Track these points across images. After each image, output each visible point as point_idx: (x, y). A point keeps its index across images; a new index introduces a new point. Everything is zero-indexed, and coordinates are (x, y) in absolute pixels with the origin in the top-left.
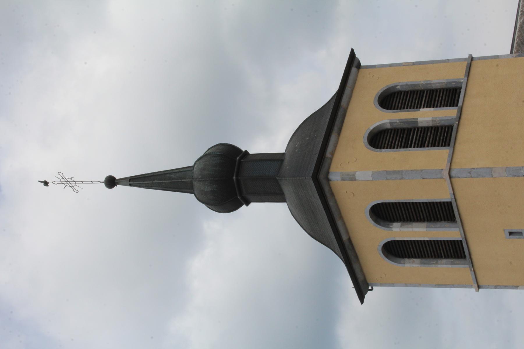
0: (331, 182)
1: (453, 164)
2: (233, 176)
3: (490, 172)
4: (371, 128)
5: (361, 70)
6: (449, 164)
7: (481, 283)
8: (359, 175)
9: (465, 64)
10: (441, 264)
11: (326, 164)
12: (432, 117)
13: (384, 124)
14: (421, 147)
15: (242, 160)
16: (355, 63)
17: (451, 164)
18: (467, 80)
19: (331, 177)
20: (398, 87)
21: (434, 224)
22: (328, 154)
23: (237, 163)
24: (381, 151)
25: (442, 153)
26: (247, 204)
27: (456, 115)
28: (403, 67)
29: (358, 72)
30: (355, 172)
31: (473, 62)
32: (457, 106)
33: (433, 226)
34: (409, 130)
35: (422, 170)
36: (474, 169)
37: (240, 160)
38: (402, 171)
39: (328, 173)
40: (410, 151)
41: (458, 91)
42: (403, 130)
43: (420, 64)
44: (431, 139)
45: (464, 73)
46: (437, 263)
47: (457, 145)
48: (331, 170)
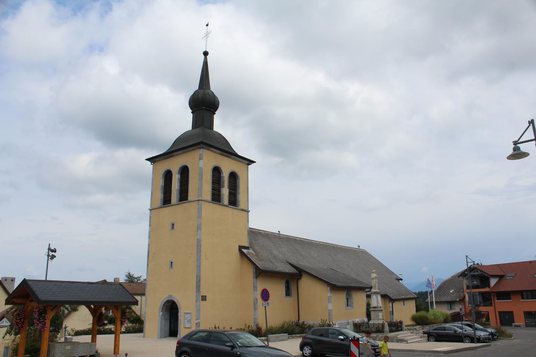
0: (199, 149)
3: (200, 217)
7: (152, 211)
8: (201, 161)
9: (246, 209)
11: (207, 147)
19: (202, 149)
22: (211, 149)
29: (246, 164)
30: (203, 160)
32: (229, 205)
34: (220, 184)
37: (211, 110)
38: (202, 180)
39: (203, 148)
41: (235, 206)
42: (220, 181)
44: (215, 193)
47: (212, 204)
48: (204, 150)
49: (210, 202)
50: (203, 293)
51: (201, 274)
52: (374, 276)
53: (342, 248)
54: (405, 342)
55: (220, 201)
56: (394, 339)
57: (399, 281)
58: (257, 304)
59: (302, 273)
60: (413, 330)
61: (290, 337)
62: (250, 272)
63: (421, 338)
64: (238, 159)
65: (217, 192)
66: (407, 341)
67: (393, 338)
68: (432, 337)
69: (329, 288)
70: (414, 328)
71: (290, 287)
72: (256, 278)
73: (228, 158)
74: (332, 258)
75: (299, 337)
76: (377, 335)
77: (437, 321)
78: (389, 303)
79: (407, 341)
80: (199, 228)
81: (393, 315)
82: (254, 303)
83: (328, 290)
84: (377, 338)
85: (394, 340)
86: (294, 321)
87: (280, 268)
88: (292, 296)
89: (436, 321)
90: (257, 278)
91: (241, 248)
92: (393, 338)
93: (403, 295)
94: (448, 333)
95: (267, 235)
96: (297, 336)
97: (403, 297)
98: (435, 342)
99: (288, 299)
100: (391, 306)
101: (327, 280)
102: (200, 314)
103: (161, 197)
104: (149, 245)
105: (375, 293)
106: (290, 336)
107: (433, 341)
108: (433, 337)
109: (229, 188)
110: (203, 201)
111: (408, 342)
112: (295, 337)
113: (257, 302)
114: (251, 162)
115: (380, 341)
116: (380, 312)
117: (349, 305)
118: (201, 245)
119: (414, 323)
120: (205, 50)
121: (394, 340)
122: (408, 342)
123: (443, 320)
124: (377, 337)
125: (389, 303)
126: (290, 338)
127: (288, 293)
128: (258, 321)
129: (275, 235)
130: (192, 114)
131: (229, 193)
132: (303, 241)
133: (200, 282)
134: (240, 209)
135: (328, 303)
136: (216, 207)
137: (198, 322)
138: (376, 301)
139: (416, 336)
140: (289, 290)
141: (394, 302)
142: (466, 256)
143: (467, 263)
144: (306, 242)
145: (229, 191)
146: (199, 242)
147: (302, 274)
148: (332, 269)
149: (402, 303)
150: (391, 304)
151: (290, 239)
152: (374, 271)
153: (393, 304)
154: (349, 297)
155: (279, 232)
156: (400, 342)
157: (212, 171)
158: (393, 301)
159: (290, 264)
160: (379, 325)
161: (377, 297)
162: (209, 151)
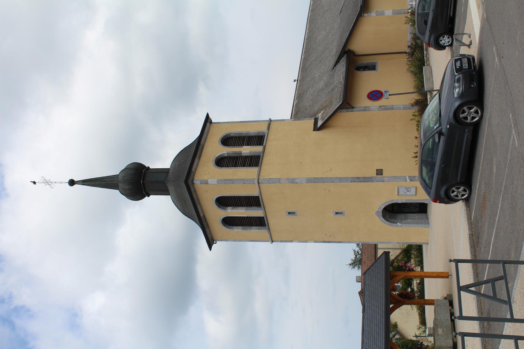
1: (260, 176)
2: (141, 181)
3: (279, 181)
4: (217, 156)
7: (273, 240)
8: (210, 181)
11: (192, 175)
16: (209, 121)
17: (259, 176)
18: (268, 132)
19: (195, 182)
20: (232, 134)
22: (193, 170)
27: (262, 150)
29: (210, 125)
30: (208, 180)
32: (263, 145)
34: (237, 157)
36: (271, 179)
38: (233, 179)
39: (193, 180)
41: (263, 137)
42: (234, 157)
44: (249, 162)
49: (260, 169)
50: (374, 174)
55: (258, 156)
58: (385, 106)
61: (427, 63)
62: (345, 116)
65: (247, 160)
69: (365, 15)
72: (353, 108)
74: (326, 12)
75: (427, 52)
80: (292, 181)
83: (368, 16)
86: (407, 59)
91: (316, 128)
96: (426, 54)
99: (379, 67)
101: (355, 17)
110: (260, 178)
112: (427, 57)
113: (384, 106)
120: (68, 183)
126: (429, 63)
127: (372, 67)
131: (248, 146)
133: (359, 177)
134: (268, 131)
135: (384, 15)
136: (266, 160)
137: (409, 179)
144: (306, 46)
146: (310, 181)
147: (348, 50)
151: (303, 67)
155: (295, 81)
159: (335, 66)
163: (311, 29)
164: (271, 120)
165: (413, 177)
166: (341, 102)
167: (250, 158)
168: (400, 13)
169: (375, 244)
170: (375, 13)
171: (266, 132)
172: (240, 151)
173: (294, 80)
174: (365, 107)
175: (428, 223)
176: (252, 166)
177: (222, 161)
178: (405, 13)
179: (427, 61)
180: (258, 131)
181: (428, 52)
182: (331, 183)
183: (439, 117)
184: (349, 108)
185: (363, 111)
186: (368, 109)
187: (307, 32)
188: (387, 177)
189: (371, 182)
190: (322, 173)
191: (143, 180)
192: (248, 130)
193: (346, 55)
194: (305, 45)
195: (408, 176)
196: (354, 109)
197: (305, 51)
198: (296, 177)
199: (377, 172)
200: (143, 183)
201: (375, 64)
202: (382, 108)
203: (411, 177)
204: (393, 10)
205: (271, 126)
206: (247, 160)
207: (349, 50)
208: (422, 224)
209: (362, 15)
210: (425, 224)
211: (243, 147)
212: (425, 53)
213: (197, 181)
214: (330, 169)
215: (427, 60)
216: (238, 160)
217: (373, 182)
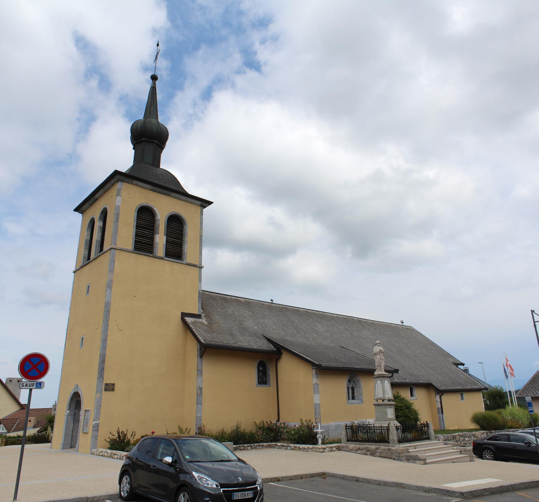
0: (117, 183)
1: (119, 251)
2: (144, 138)
3: (112, 271)
4: (154, 209)
5: (199, 208)
6: (120, 249)
7: (76, 273)
8: (119, 198)
9: (198, 264)
10: (85, 251)
11: (128, 180)
12: (158, 243)
13: (157, 216)
14: (136, 234)
15: (155, 144)
16: (204, 204)
17: (120, 250)
18: (184, 264)
19: (120, 183)
20: (185, 226)
21: (99, 244)
22: (135, 182)
23: (154, 141)
24: (135, 212)
25: (130, 244)
26: (134, 149)
27: (158, 255)
28: (199, 230)
29: (199, 205)
30: (121, 196)
31: (198, 268)
32: (165, 257)
33: (97, 244)
34: (153, 230)
35: (117, 233)
36: (114, 262)
37: (155, 142)
38: (118, 222)
39: (122, 181)
40: (134, 228)
41: (179, 259)
42: (153, 227)
43: (200, 239)
44: (144, 241)
45: (190, 263)
46: (85, 248)
47: (135, 254)
48: (124, 183)
49: (131, 252)
50: (108, 380)
51: (107, 352)
52: (378, 350)
53: (374, 323)
54: (420, 462)
55: (152, 252)
56: (401, 455)
57: (457, 367)
58: (202, 395)
59: (282, 351)
60: (471, 437)
61: (248, 446)
62: (193, 349)
63: (461, 454)
64: (193, 201)
65: (148, 240)
66: (425, 460)
67: (400, 453)
68: (487, 452)
69: (314, 370)
70: (473, 435)
71: (267, 371)
72: (201, 357)
73: (180, 201)
74: (351, 334)
75: (266, 447)
76: (377, 447)
77: (517, 424)
78: (436, 395)
79: (425, 460)
80: (109, 286)
81: (442, 413)
82: (197, 393)
83: (313, 374)
84: (377, 453)
85: (402, 457)
86: (267, 422)
87: (243, 343)
88: (270, 384)
89: (515, 424)
90: (203, 358)
91: (184, 315)
92: (400, 453)
93: (460, 384)
94: (515, 446)
95: (226, 299)
96: (263, 446)
97: (460, 387)
98: (493, 460)
99: (263, 388)
100: (439, 400)
101: (312, 359)
102: (100, 412)
103: (84, 254)
104: (69, 318)
105: (379, 377)
106: (249, 445)
107: (491, 459)
108: (490, 452)
109: (167, 235)
110: (117, 251)
111: (427, 461)
112: (258, 447)
113: (202, 393)
114: (206, 203)
115: (382, 457)
116: (388, 407)
117: (356, 397)
118: (109, 311)
119: (477, 427)
120: (154, 74)
121: (402, 457)
122: (427, 461)
123: (527, 422)
124: (377, 450)
125: (436, 395)
126: (248, 449)
127: (263, 380)
128: (202, 421)
129: (262, 304)
130: (134, 151)
131: (166, 242)
132: (310, 313)
133: (104, 362)
134: (185, 263)
135: (314, 393)
136: (143, 260)
137: (95, 424)
138: (381, 390)
139: (453, 449)
140: (266, 377)
141: (442, 395)
142: (532, 310)
143: (534, 322)
144: (315, 314)
145: (166, 238)
146: (108, 305)
147: (282, 352)
148: (343, 347)
149: (459, 396)
150: (438, 398)
151: (287, 309)
152: (378, 341)
153: (442, 396)
154: (355, 384)
155: (272, 300)
156: (411, 461)
157: (138, 212)
158: (442, 394)
159: (267, 338)
160: (381, 429)
161: (383, 383)
162: (132, 185)
163: (336, 318)
164: (201, 268)
165: (98, 428)
166: (203, 342)
167: (150, 243)
168: (315, 414)
169: (353, 398)
170: (316, 383)
171: (184, 262)
172: (159, 233)
173: (272, 299)
174: (202, 371)
175: (64, 448)
176: (135, 244)
177: (179, 222)
178: (316, 418)
179: (251, 446)
180: (186, 253)
181: (266, 448)
182: (102, 330)
183: (220, 460)
184: (201, 353)
185: (197, 368)
186: (199, 374)
187: (333, 315)
188: (100, 397)
189: (98, 377)
190: (116, 320)
191: (145, 141)
192: (188, 243)
193: (275, 350)
194: (317, 312)
195: (99, 423)
196: (199, 358)
197: (308, 312)
198: (113, 290)
199: (110, 384)
200: (142, 141)
201: (268, 384)
202: (199, 391)
203: (98, 426)
204: (319, 405)
205: (193, 267)
206: (148, 240)
207: (282, 354)
208: (65, 440)
209: (314, 368)
210: (64, 444)
211: (165, 236)
212: (265, 444)
213: (119, 185)
214: (121, 329)
215: (253, 447)
216: (148, 231)
217: (98, 379)
